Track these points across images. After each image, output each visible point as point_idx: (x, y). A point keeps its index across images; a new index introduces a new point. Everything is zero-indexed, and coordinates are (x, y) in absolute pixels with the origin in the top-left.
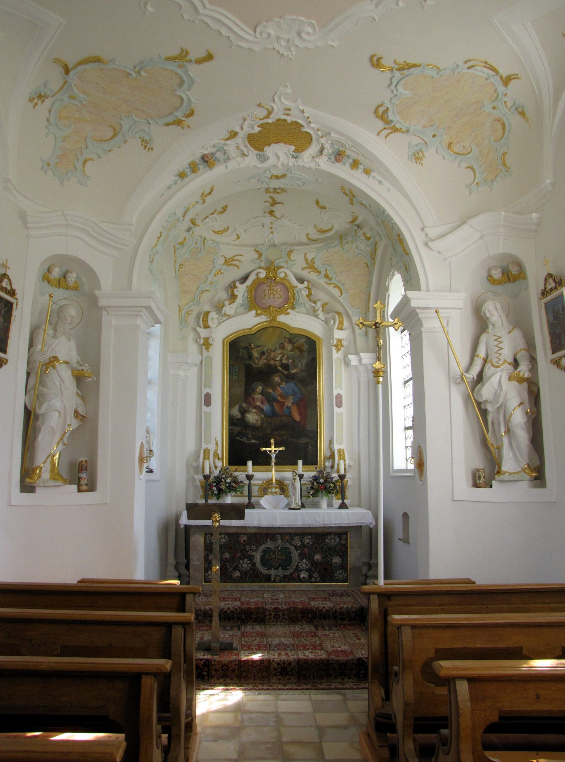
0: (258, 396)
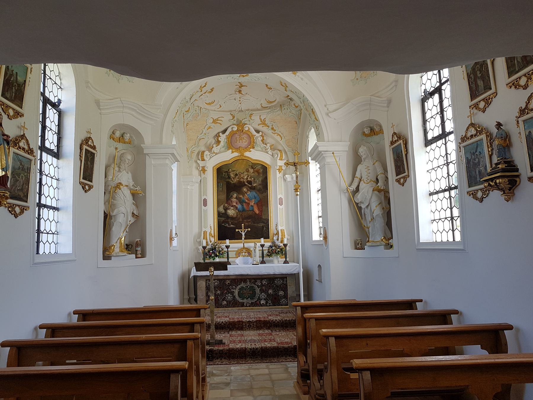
0: (234, 200)
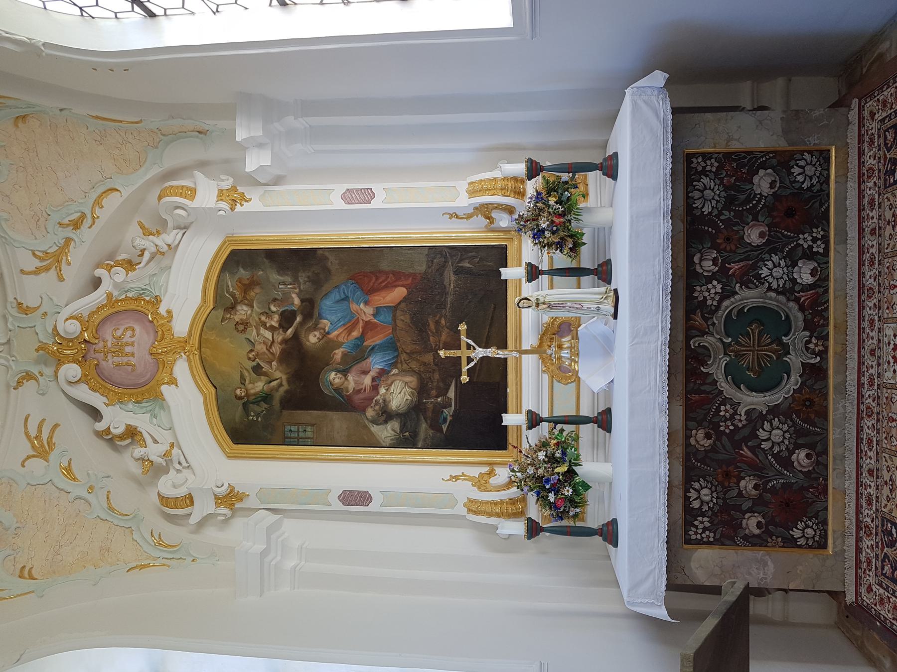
0: (351, 382)
